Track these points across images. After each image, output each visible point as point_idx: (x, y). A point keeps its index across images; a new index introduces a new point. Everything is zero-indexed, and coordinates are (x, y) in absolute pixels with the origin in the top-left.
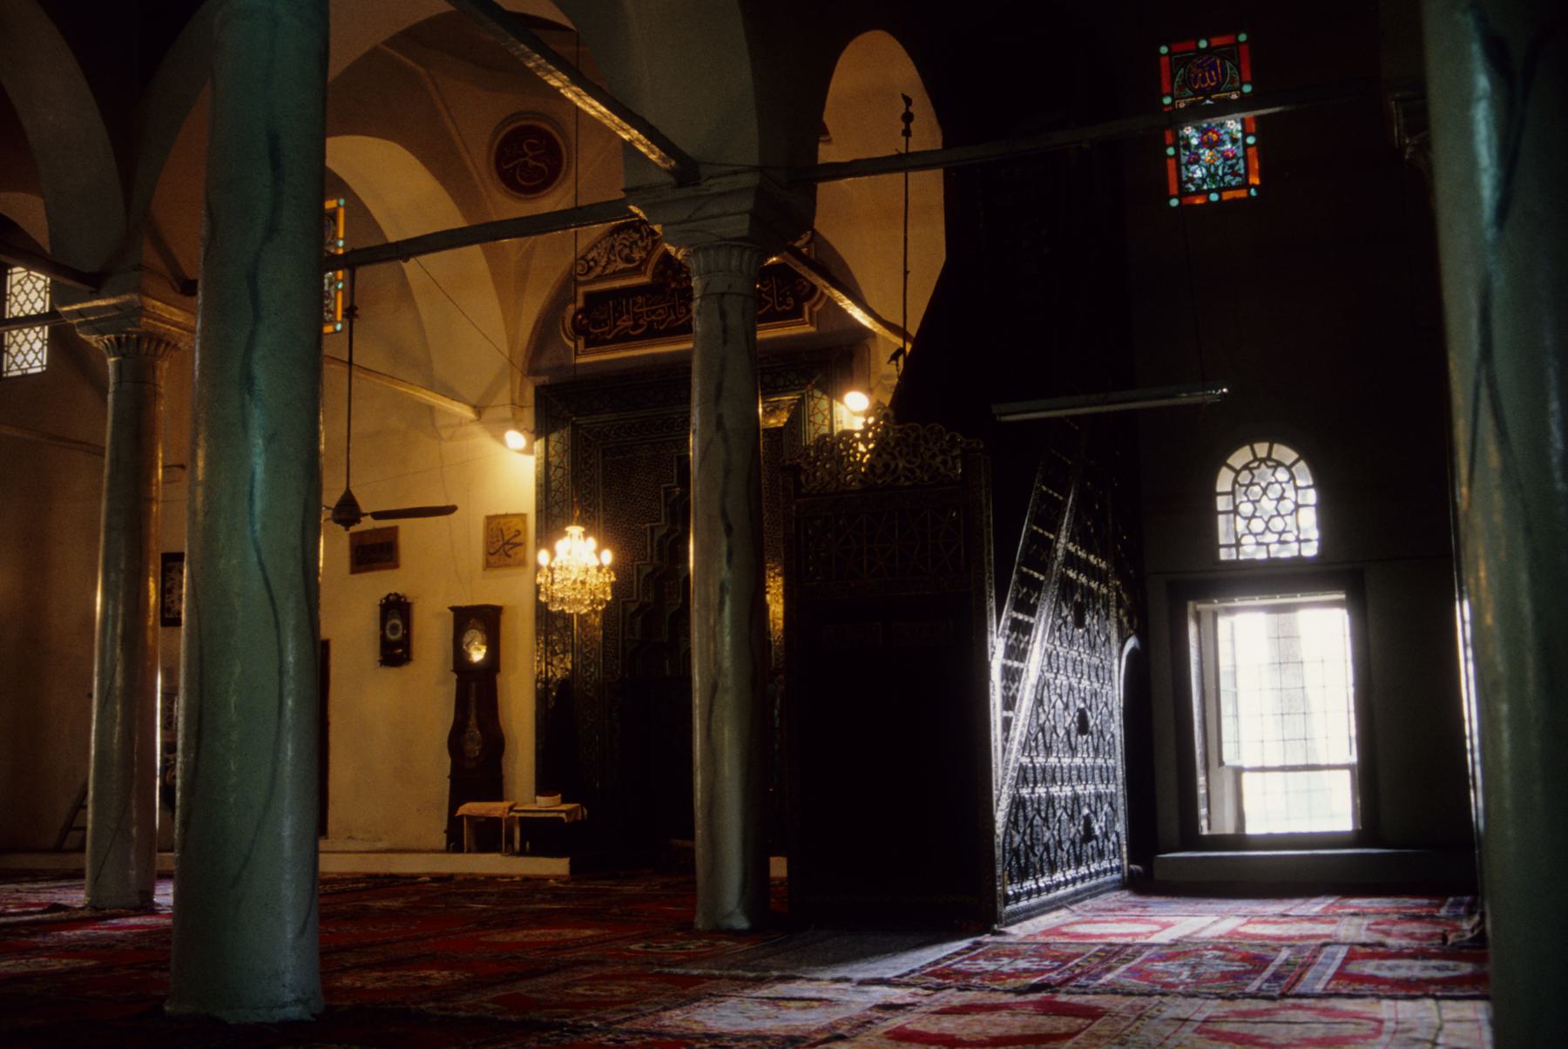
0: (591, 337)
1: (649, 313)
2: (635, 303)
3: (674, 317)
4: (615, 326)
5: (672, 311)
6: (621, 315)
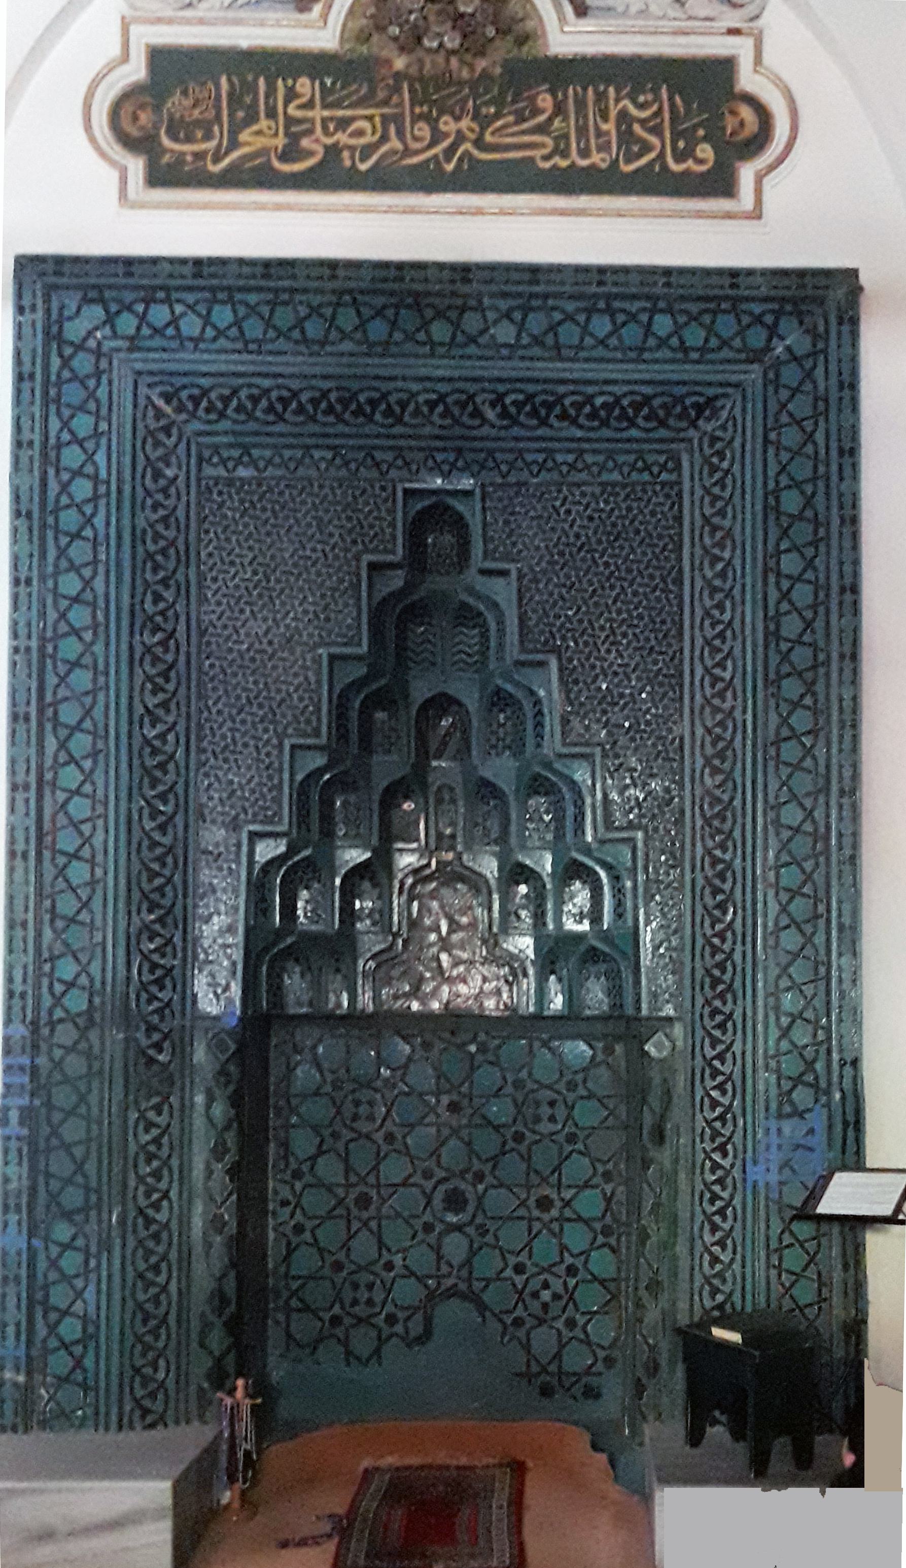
0: (166, 158)
1: (332, 127)
2: (291, 94)
3: (399, 146)
4: (234, 144)
5: (392, 129)
6: (252, 118)
